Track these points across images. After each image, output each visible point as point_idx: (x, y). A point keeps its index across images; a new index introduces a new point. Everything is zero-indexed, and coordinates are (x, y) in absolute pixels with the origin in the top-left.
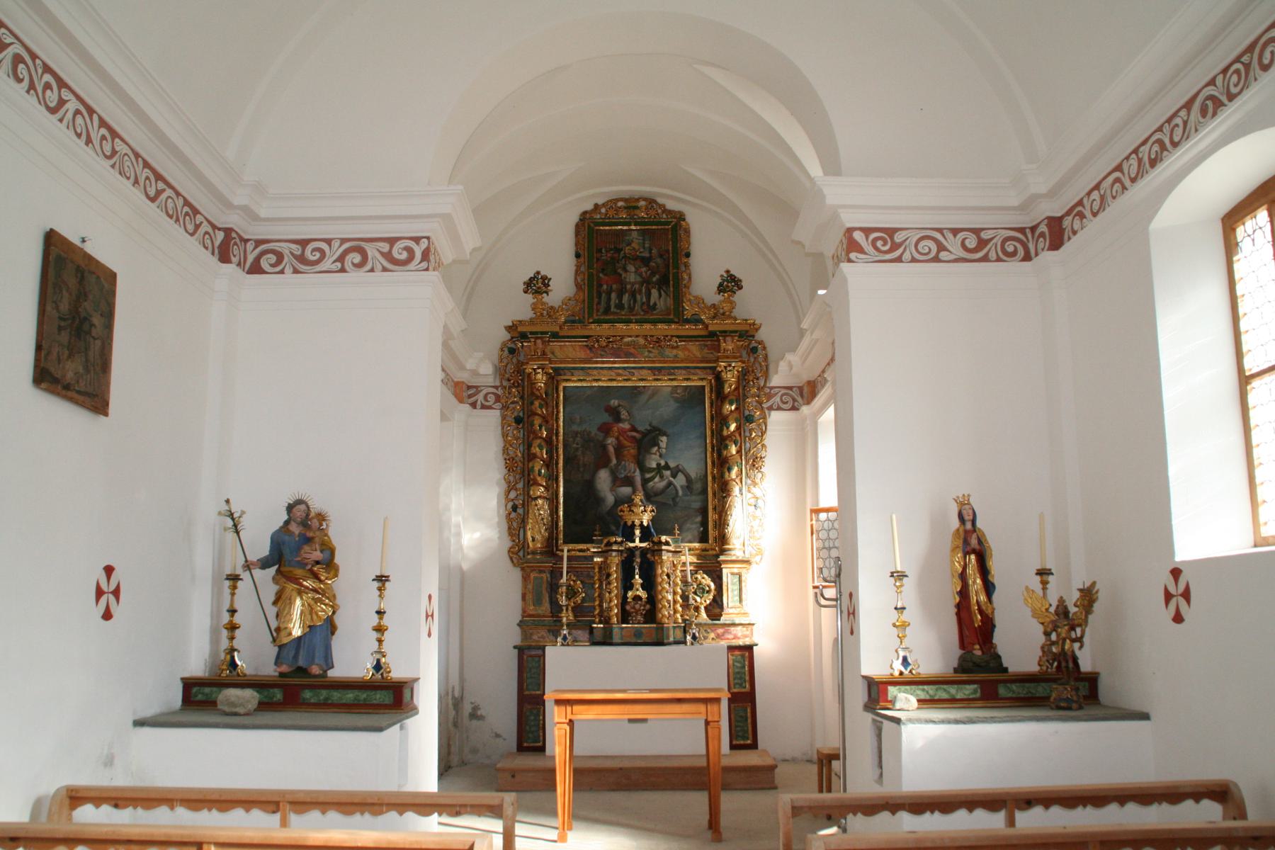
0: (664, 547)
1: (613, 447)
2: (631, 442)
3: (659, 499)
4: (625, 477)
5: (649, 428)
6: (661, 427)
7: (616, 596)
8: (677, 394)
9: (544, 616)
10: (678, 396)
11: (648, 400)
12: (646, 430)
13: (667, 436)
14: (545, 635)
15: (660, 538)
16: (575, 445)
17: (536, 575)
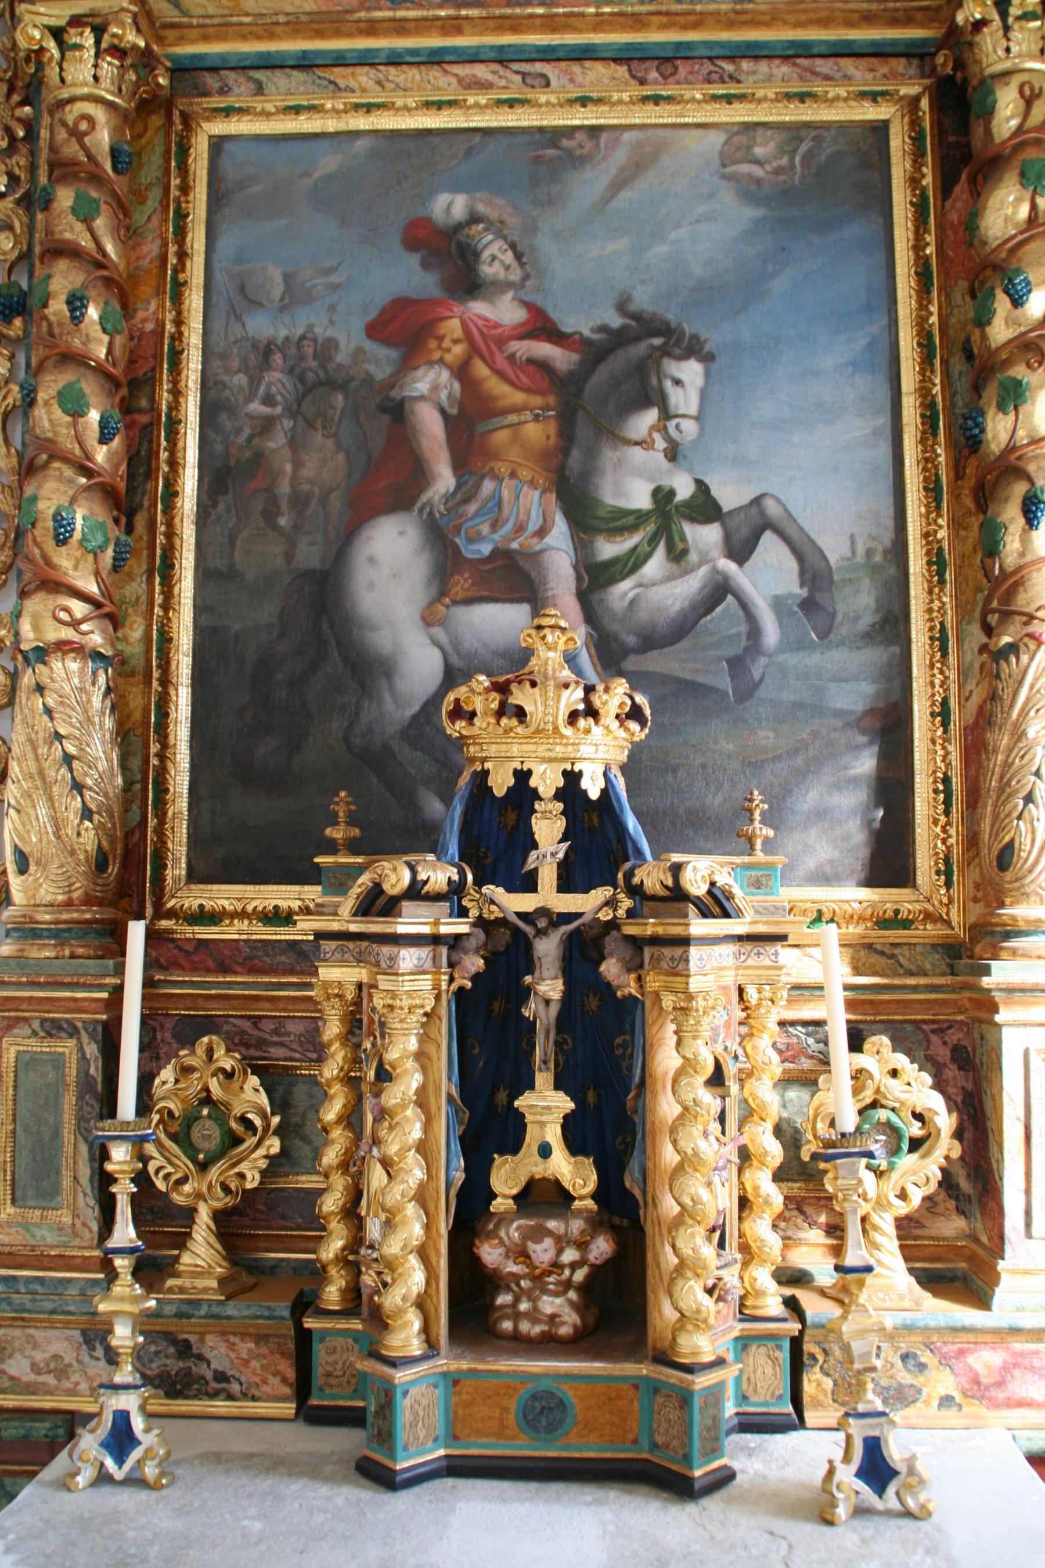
0: (698, 926)
1: (443, 412)
2: (527, 390)
3: (656, 662)
4: (495, 553)
5: (616, 321)
6: (671, 317)
7: (421, 1197)
8: (757, 162)
9: (65, 1262)
10: (757, 171)
11: (617, 186)
12: (603, 329)
13: (708, 359)
14: (69, 1357)
15: (676, 869)
16: (256, 407)
17: (35, 1046)
